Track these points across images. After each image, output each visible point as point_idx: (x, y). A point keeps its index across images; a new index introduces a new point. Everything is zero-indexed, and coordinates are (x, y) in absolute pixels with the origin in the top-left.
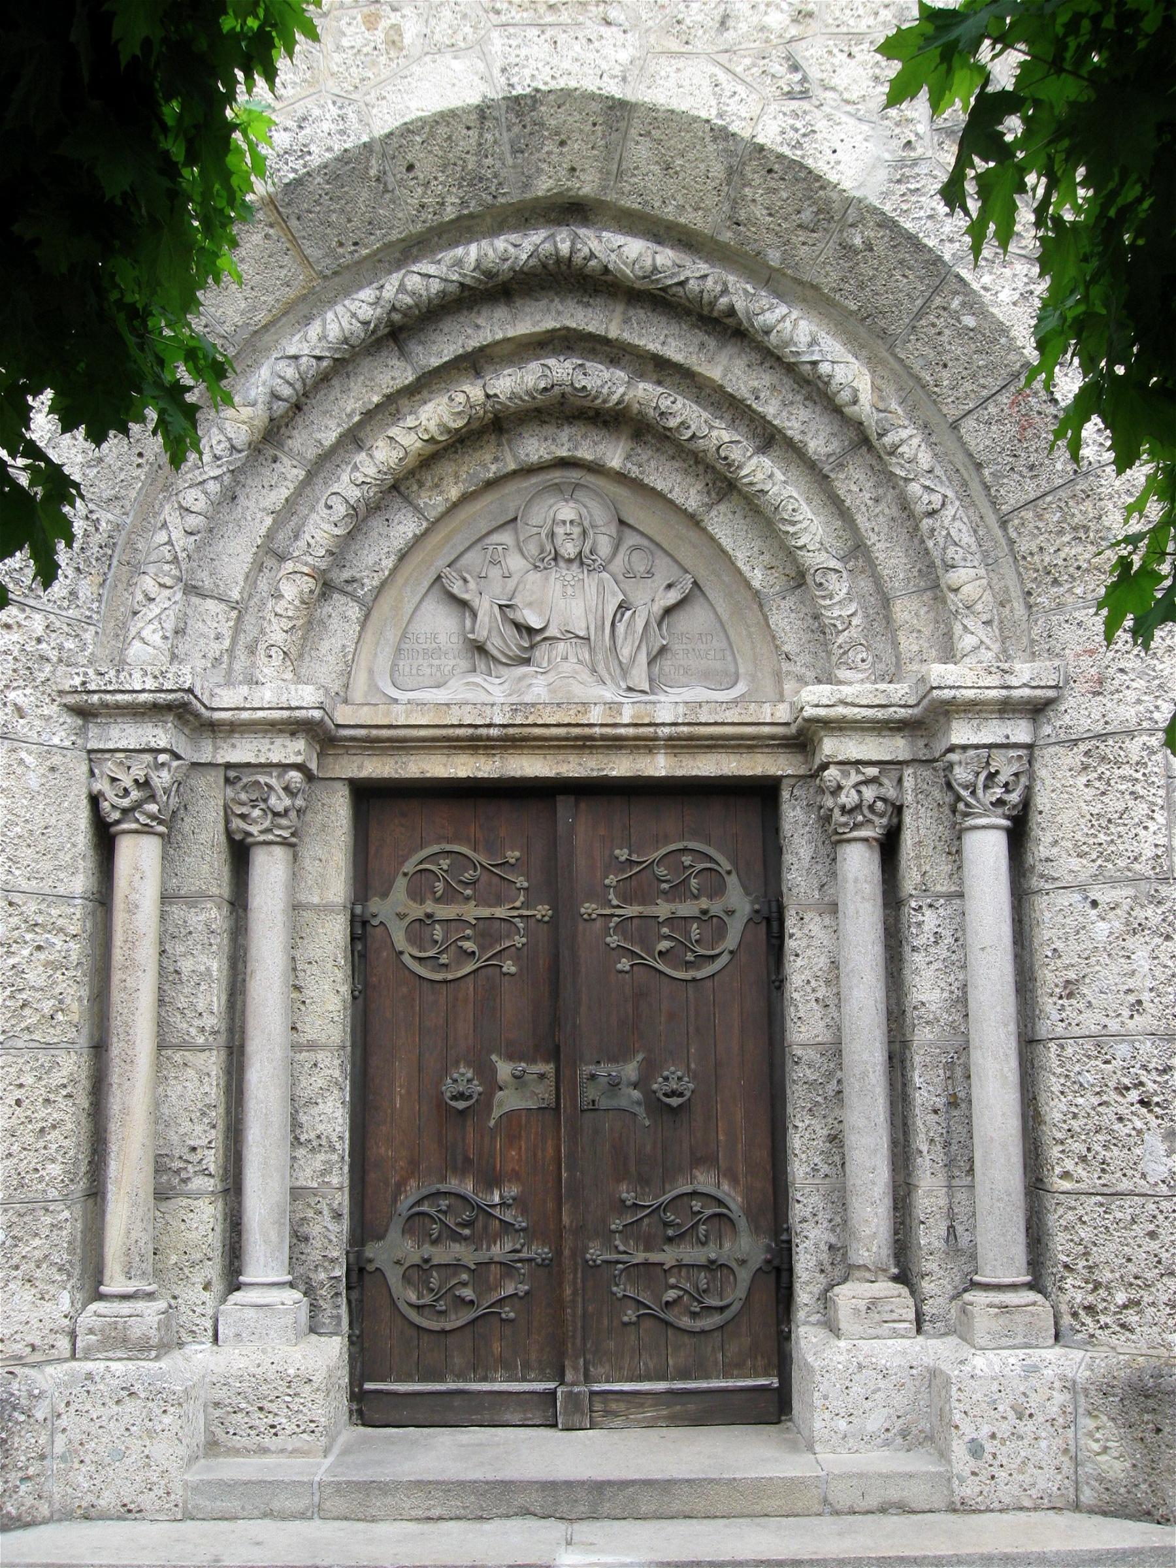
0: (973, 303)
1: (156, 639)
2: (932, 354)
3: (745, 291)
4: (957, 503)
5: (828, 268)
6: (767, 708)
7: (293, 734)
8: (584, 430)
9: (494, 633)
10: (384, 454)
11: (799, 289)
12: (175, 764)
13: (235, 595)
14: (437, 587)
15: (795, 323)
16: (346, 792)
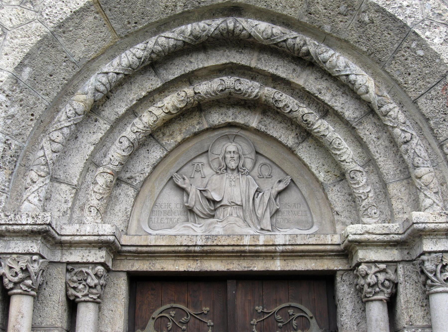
0: (422, 44)
1: (36, 201)
2: (403, 69)
3: (314, 44)
4: (418, 138)
5: (353, 32)
6: (329, 237)
7: (100, 248)
8: (239, 110)
9: (198, 203)
10: (147, 119)
11: (339, 43)
12: (41, 261)
13: (75, 182)
14: (171, 182)
15: (338, 58)
16: (126, 278)
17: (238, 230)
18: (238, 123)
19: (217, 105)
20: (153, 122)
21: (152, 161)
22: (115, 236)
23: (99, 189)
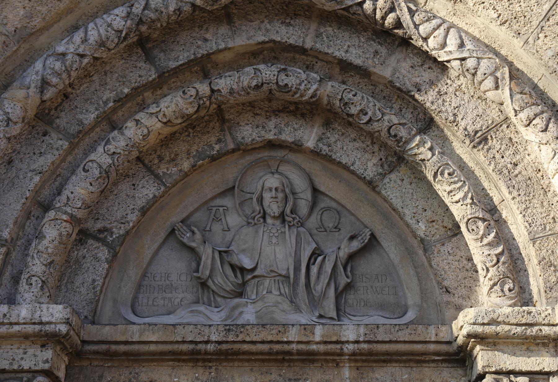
6: (432, 330)
8: (286, 119)
17: (280, 317)
18: (284, 141)
19: (250, 111)
20: (141, 137)
21: (139, 202)
22: (70, 325)
23: (47, 247)
